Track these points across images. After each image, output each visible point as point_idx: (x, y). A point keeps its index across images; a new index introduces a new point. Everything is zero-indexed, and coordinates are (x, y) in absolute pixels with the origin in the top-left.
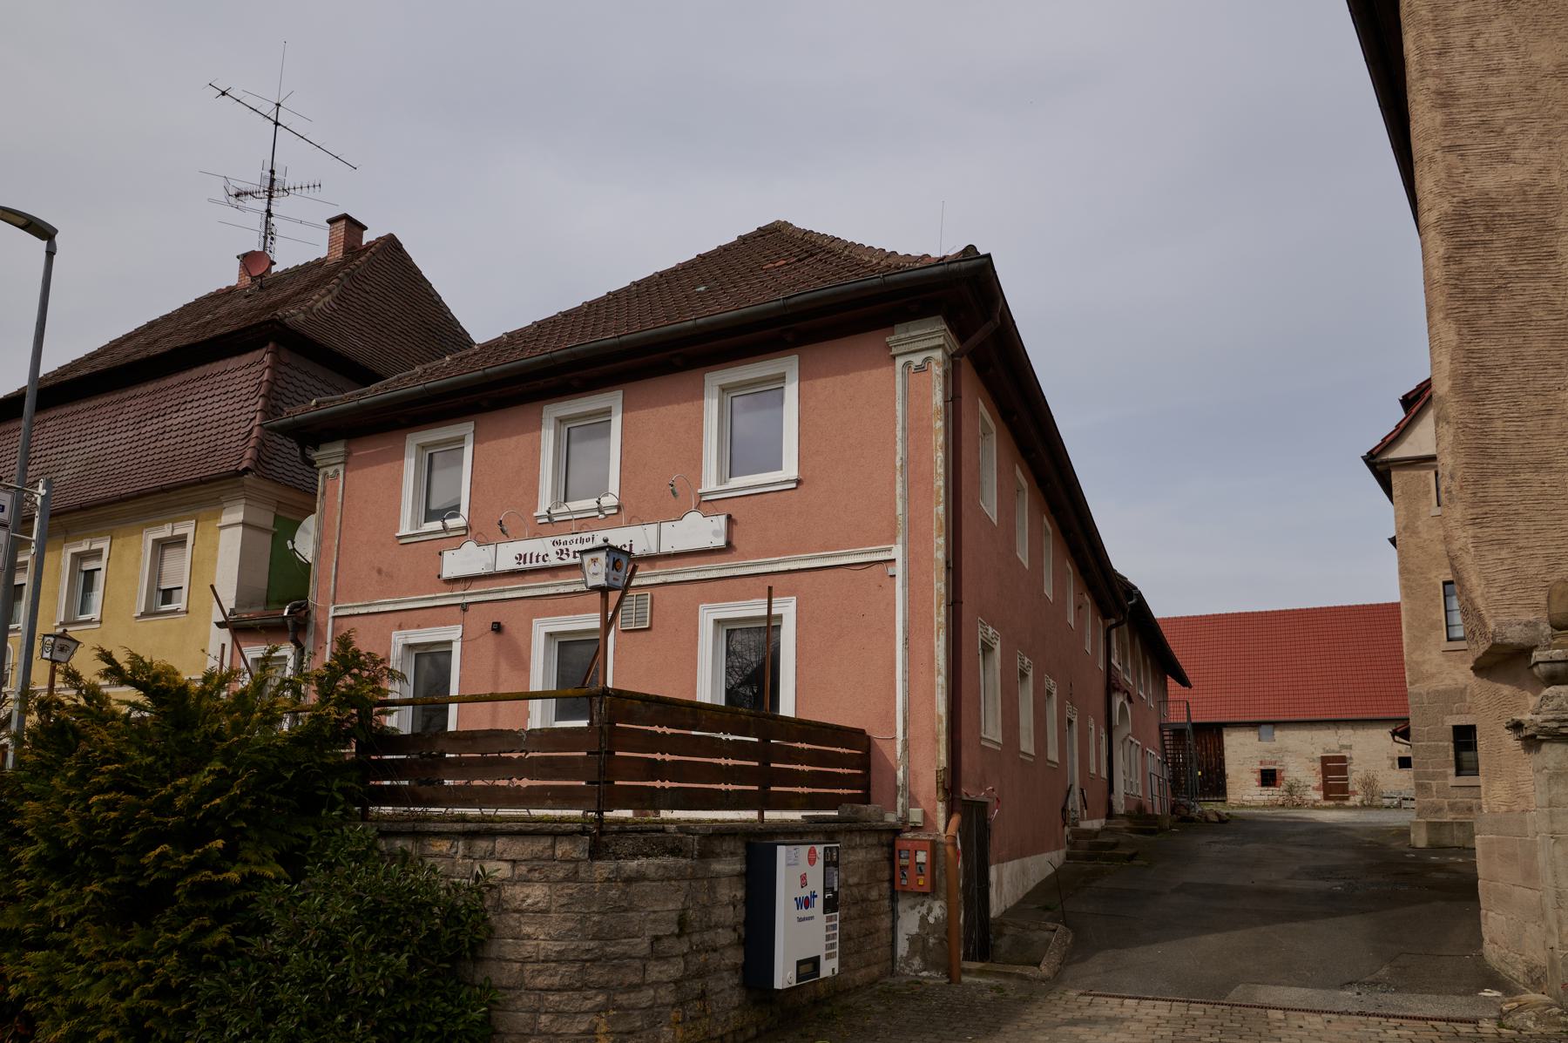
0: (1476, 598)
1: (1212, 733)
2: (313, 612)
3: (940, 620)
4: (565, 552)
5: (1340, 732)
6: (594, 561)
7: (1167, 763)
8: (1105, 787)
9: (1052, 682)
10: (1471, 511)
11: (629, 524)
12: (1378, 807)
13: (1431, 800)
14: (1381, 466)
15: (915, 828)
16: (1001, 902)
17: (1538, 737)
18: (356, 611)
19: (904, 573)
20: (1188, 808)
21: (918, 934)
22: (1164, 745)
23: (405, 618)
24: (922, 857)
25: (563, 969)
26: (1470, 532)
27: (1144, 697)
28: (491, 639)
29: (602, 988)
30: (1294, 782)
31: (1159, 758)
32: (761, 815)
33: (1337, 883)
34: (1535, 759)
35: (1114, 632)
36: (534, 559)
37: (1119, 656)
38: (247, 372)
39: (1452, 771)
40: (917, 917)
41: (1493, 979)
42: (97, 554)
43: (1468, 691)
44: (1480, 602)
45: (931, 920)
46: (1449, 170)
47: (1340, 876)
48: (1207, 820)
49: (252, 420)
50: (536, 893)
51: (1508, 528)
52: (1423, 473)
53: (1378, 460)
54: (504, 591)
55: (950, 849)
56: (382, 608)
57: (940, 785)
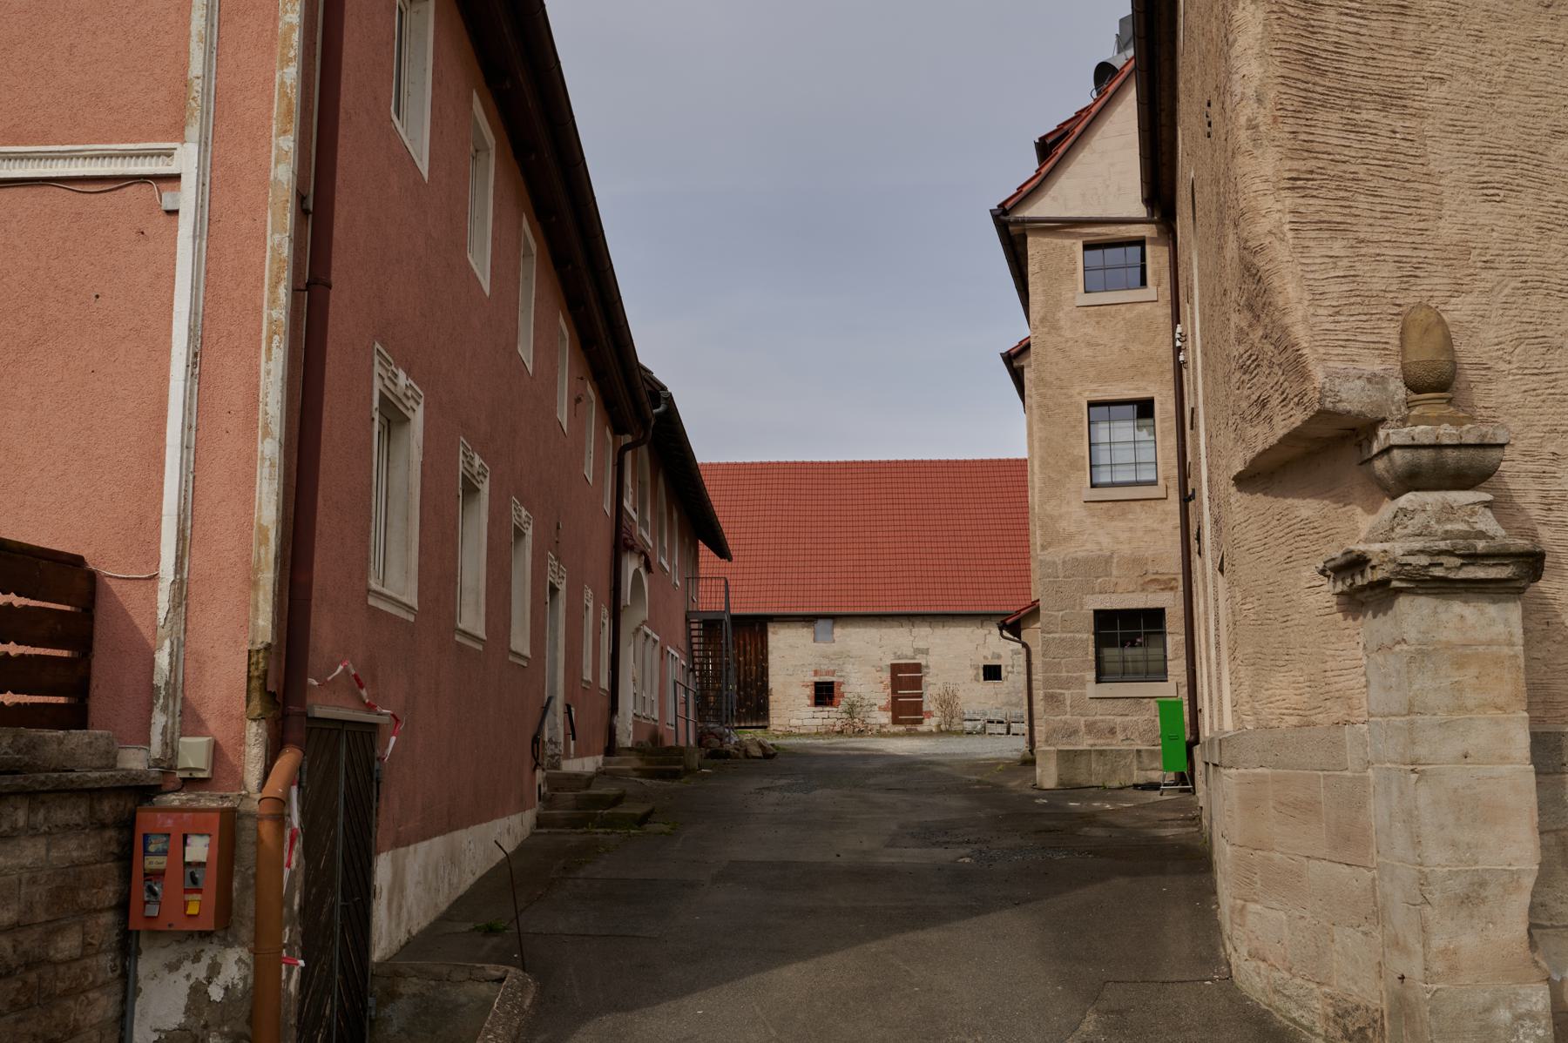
0: (1294, 324)
1: (755, 628)
3: (275, 314)
5: (916, 631)
7: (693, 670)
8: (604, 703)
9: (524, 513)
10: (1289, 164)
13: (1063, 718)
15: (192, 783)
16: (398, 925)
17: (1395, 584)
19: (199, 207)
20: (721, 737)
21: (182, 1028)
22: (691, 644)
24: (198, 849)
26: (1288, 202)
27: (668, 568)
30: (856, 699)
31: (683, 663)
33: (961, 851)
34: (1373, 626)
35: (629, 455)
37: (634, 500)
39: (1092, 675)
40: (183, 987)
43: (1115, 561)
44: (1300, 333)
45: (216, 993)
47: (960, 839)
48: (747, 755)
51: (1343, 203)
52: (1067, 242)
53: (1011, 217)
55: (267, 828)
57: (255, 683)
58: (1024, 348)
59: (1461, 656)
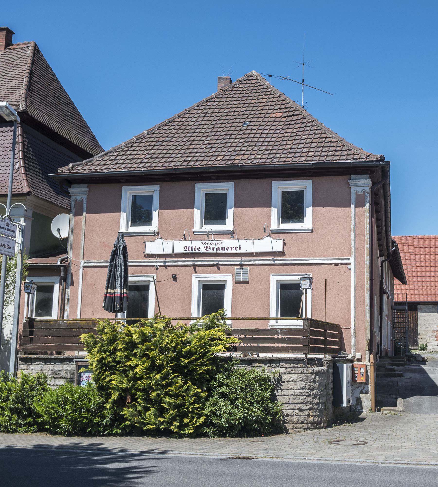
4: (208, 247)
25: (301, 397)
32: (306, 357)
35: (384, 263)
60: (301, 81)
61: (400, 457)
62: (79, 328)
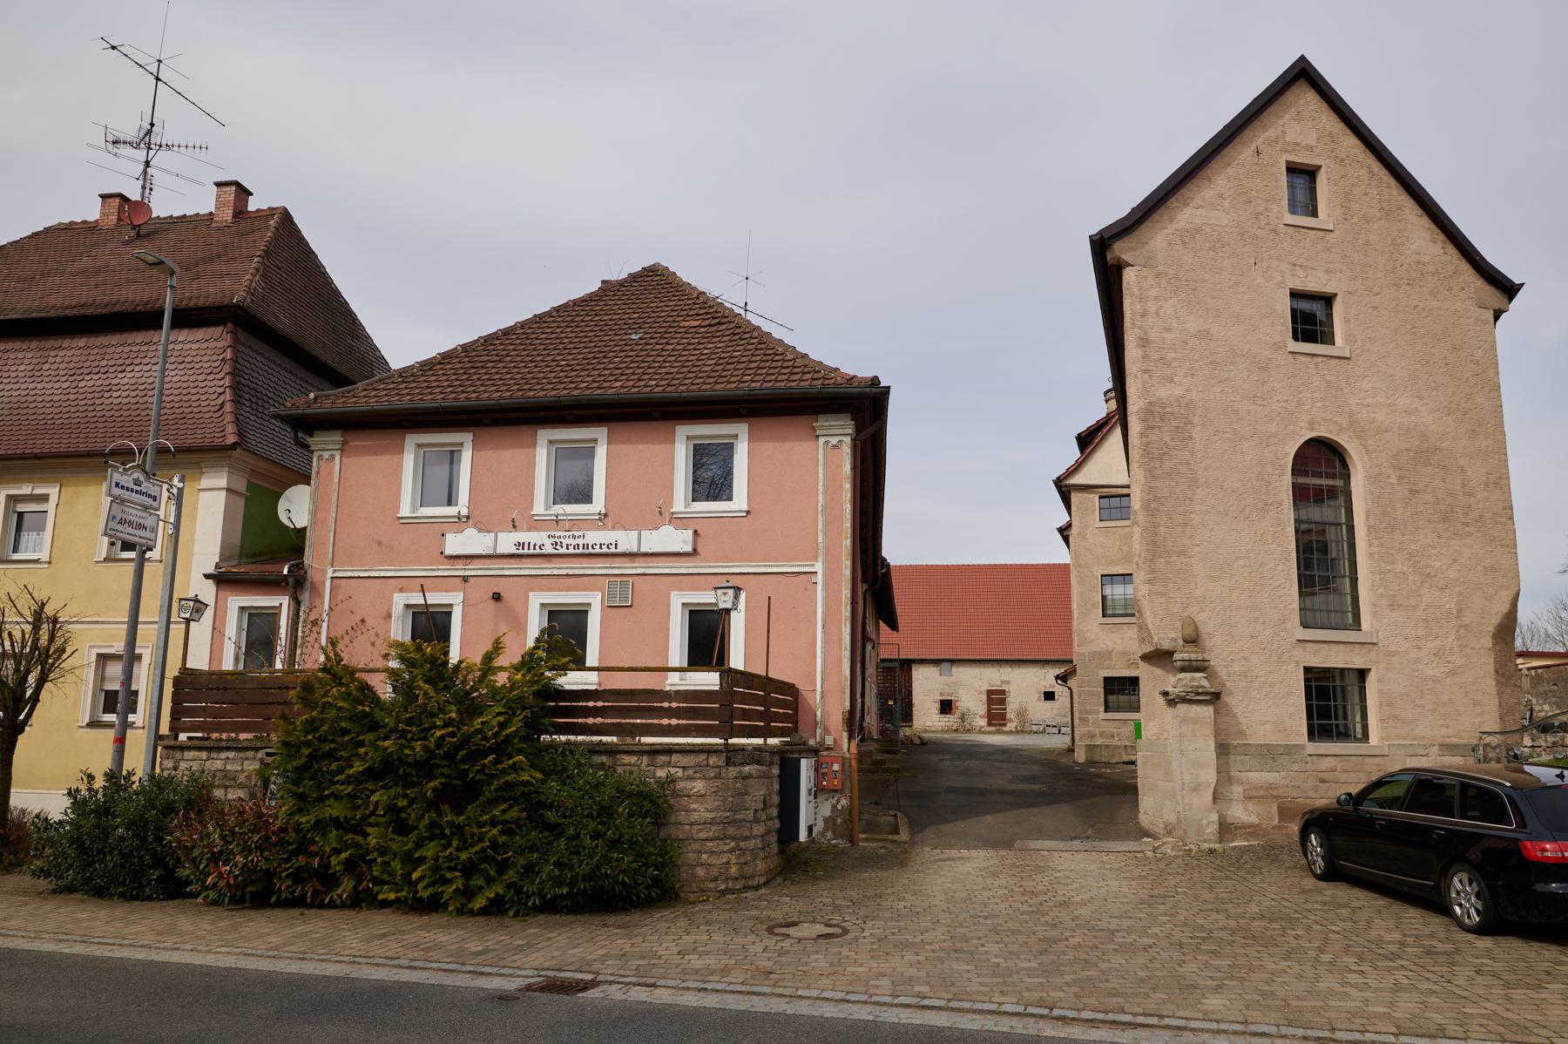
1: (907, 665)
2: (309, 572)
5: (1002, 670)
6: (725, 594)
11: (614, 528)
12: (1030, 732)
14: (1064, 489)
15: (828, 749)
18: (356, 574)
23: (403, 583)
24: (836, 767)
25: (714, 828)
28: (491, 605)
29: (733, 839)
32: (765, 741)
34: (1171, 711)
36: (532, 547)
38: (205, 346)
39: (1102, 708)
40: (830, 805)
41: (1147, 834)
42: (44, 498)
44: (1150, 626)
45: (839, 807)
46: (1144, 383)
49: (220, 394)
50: (699, 786)
52: (1091, 496)
54: (503, 569)
56: (383, 574)
58: (1069, 526)
59: (1196, 721)
60: (743, 305)
61: (928, 983)
62: (280, 688)
